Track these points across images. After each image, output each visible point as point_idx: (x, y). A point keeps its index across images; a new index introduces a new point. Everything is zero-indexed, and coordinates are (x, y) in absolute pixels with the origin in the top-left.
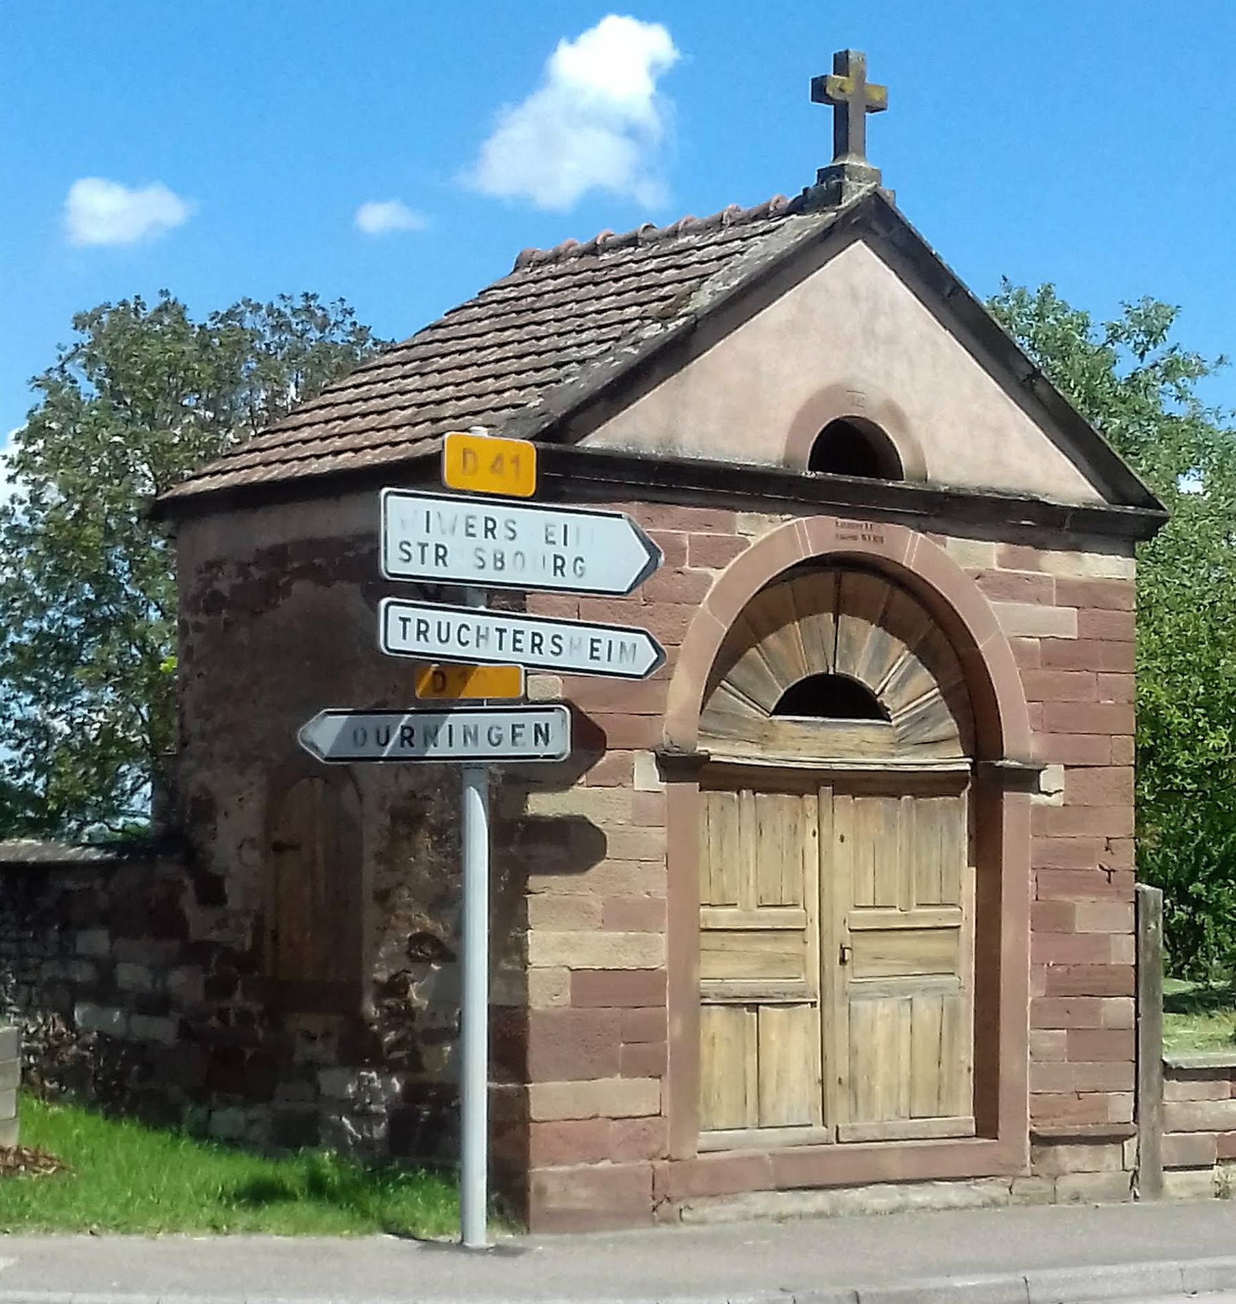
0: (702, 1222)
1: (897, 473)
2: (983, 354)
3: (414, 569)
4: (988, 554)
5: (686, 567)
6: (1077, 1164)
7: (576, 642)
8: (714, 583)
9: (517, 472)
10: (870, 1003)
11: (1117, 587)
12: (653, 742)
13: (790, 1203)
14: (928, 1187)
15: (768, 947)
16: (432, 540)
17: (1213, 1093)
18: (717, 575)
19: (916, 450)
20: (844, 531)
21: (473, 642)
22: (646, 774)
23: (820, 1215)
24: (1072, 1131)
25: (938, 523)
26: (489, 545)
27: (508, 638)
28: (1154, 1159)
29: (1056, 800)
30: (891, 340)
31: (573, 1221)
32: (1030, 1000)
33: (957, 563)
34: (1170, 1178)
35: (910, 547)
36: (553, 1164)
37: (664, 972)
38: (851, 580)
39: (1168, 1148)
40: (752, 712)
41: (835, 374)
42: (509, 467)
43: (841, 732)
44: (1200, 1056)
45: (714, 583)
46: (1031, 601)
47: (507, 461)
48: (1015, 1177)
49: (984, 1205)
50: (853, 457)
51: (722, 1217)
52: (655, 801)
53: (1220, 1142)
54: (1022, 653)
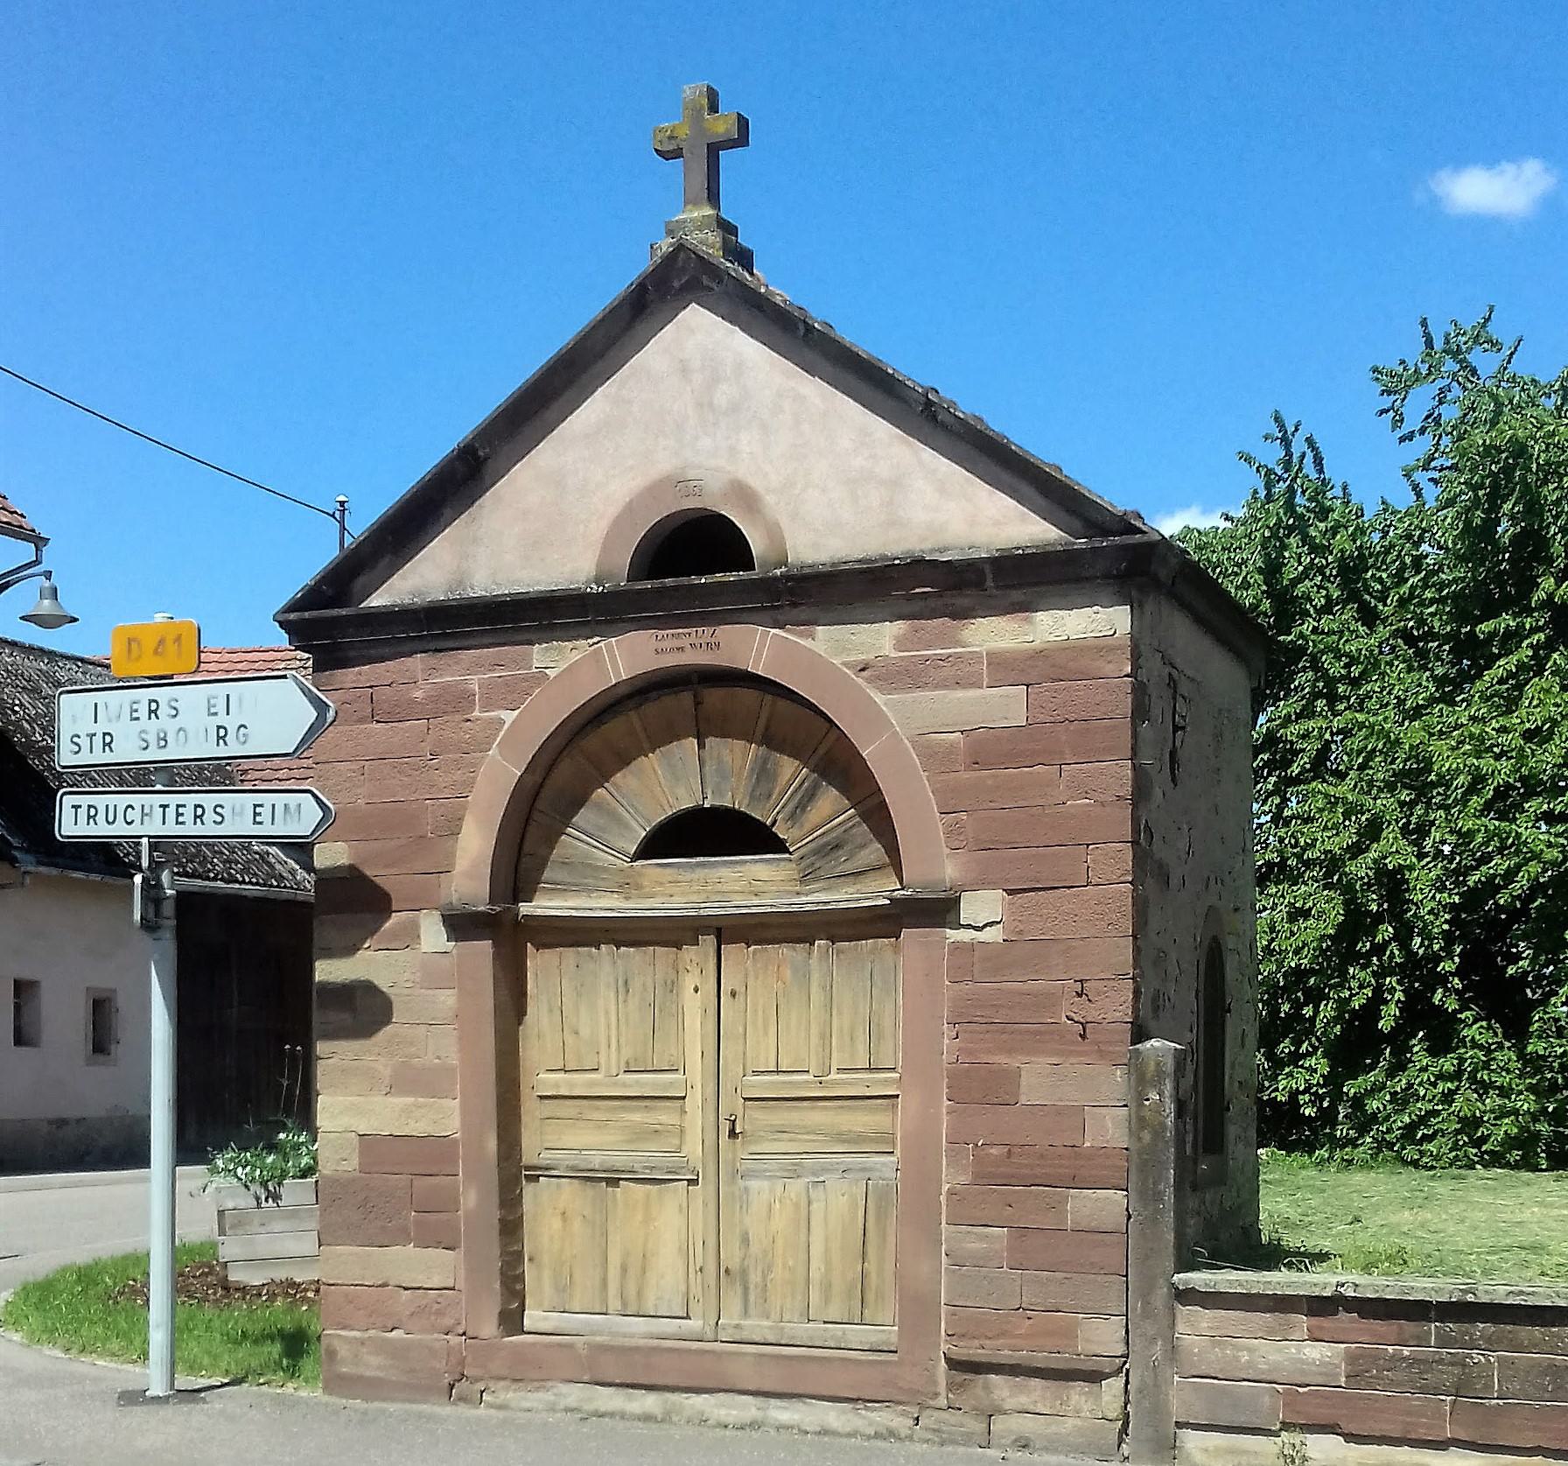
0: (500, 1407)
1: (746, 561)
2: (550, 414)
3: (85, 758)
4: (881, 638)
5: (476, 713)
6: (1023, 1400)
7: (237, 809)
9: (179, 654)
10: (766, 1184)
11: (1099, 648)
12: (443, 901)
13: (609, 1399)
14: (797, 1405)
16: (100, 729)
17: (1271, 1331)
18: (509, 717)
19: (775, 534)
20: (667, 644)
21: (138, 821)
22: (433, 934)
23: (647, 1418)
24: (1006, 1356)
25: (803, 613)
26: (153, 726)
27: (171, 812)
28: (1157, 1411)
29: (993, 935)
30: (735, 408)
31: (338, 1384)
32: (946, 1187)
33: (827, 658)
34: (1192, 1441)
35: (756, 647)
36: (343, 1328)
37: (456, 1140)
38: (714, 697)
39: (1180, 1398)
40: (605, 858)
41: (664, 464)
42: (171, 648)
43: (725, 872)
44: (1427, 1283)
46: (946, 687)
47: (169, 642)
48: (922, 1407)
49: (877, 1436)
50: (692, 553)
51: (527, 1405)
52: (445, 960)
53: (1291, 1400)
54: (935, 757)
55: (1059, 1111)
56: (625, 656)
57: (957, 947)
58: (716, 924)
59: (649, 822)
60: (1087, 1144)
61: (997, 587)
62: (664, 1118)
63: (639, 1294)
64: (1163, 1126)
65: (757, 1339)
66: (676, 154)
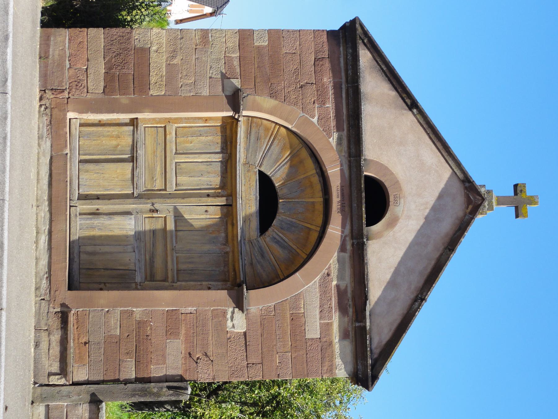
8: (311, 119)
15: (159, 169)
18: (315, 120)
19: (379, 235)
28: (52, 398)
31: (45, 43)
35: (335, 230)
45: (311, 119)
50: (373, 200)
54: (297, 298)
55: (164, 356)
56: (335, 172)
57: (225, 313)
58: (234, 204)
59: (272, 176)
60: (152, 367)
61: (355, 326)
62: (158, 181)
63: (87, 171)
64: (159, 396)
65: (71, 224)
66: (516, 193)
